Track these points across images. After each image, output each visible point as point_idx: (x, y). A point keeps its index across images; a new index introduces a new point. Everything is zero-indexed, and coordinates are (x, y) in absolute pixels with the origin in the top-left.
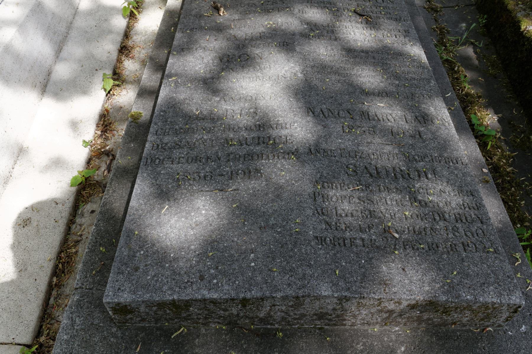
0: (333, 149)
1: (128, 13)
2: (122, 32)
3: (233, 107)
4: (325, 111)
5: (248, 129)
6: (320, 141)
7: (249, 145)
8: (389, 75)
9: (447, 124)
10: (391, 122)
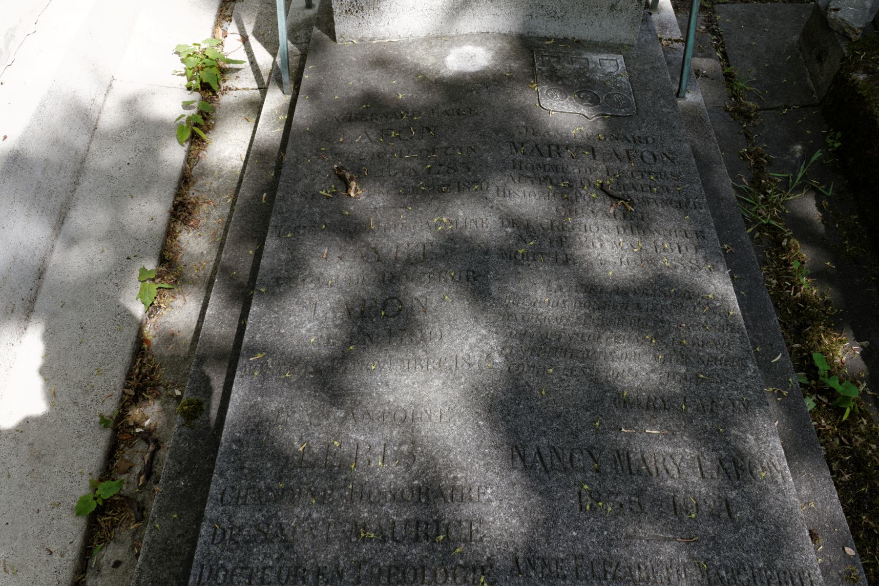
0: (562, 556)
1: (188, 134)
2: (176, 174)
3: (370, 439)
4: (545, 452)
5: (398, 498)
6: (536, 536)
7: (398, 542)
8: (667, 352)
9: (780, 480)
10: (673, 477)
